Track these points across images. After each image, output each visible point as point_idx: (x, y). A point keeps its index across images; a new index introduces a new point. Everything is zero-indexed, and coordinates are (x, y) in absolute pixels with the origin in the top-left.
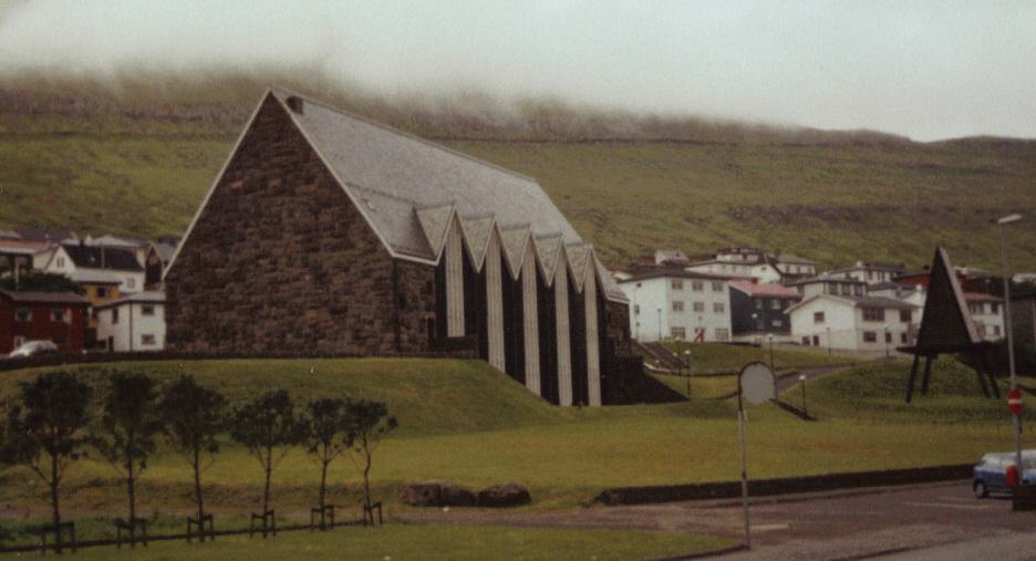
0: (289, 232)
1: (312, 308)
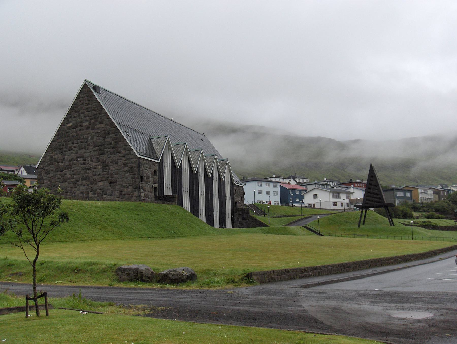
0: (91, 146)
1: (101, 181)
